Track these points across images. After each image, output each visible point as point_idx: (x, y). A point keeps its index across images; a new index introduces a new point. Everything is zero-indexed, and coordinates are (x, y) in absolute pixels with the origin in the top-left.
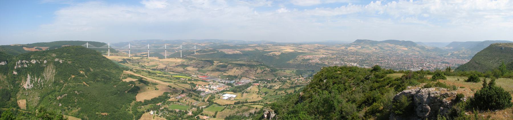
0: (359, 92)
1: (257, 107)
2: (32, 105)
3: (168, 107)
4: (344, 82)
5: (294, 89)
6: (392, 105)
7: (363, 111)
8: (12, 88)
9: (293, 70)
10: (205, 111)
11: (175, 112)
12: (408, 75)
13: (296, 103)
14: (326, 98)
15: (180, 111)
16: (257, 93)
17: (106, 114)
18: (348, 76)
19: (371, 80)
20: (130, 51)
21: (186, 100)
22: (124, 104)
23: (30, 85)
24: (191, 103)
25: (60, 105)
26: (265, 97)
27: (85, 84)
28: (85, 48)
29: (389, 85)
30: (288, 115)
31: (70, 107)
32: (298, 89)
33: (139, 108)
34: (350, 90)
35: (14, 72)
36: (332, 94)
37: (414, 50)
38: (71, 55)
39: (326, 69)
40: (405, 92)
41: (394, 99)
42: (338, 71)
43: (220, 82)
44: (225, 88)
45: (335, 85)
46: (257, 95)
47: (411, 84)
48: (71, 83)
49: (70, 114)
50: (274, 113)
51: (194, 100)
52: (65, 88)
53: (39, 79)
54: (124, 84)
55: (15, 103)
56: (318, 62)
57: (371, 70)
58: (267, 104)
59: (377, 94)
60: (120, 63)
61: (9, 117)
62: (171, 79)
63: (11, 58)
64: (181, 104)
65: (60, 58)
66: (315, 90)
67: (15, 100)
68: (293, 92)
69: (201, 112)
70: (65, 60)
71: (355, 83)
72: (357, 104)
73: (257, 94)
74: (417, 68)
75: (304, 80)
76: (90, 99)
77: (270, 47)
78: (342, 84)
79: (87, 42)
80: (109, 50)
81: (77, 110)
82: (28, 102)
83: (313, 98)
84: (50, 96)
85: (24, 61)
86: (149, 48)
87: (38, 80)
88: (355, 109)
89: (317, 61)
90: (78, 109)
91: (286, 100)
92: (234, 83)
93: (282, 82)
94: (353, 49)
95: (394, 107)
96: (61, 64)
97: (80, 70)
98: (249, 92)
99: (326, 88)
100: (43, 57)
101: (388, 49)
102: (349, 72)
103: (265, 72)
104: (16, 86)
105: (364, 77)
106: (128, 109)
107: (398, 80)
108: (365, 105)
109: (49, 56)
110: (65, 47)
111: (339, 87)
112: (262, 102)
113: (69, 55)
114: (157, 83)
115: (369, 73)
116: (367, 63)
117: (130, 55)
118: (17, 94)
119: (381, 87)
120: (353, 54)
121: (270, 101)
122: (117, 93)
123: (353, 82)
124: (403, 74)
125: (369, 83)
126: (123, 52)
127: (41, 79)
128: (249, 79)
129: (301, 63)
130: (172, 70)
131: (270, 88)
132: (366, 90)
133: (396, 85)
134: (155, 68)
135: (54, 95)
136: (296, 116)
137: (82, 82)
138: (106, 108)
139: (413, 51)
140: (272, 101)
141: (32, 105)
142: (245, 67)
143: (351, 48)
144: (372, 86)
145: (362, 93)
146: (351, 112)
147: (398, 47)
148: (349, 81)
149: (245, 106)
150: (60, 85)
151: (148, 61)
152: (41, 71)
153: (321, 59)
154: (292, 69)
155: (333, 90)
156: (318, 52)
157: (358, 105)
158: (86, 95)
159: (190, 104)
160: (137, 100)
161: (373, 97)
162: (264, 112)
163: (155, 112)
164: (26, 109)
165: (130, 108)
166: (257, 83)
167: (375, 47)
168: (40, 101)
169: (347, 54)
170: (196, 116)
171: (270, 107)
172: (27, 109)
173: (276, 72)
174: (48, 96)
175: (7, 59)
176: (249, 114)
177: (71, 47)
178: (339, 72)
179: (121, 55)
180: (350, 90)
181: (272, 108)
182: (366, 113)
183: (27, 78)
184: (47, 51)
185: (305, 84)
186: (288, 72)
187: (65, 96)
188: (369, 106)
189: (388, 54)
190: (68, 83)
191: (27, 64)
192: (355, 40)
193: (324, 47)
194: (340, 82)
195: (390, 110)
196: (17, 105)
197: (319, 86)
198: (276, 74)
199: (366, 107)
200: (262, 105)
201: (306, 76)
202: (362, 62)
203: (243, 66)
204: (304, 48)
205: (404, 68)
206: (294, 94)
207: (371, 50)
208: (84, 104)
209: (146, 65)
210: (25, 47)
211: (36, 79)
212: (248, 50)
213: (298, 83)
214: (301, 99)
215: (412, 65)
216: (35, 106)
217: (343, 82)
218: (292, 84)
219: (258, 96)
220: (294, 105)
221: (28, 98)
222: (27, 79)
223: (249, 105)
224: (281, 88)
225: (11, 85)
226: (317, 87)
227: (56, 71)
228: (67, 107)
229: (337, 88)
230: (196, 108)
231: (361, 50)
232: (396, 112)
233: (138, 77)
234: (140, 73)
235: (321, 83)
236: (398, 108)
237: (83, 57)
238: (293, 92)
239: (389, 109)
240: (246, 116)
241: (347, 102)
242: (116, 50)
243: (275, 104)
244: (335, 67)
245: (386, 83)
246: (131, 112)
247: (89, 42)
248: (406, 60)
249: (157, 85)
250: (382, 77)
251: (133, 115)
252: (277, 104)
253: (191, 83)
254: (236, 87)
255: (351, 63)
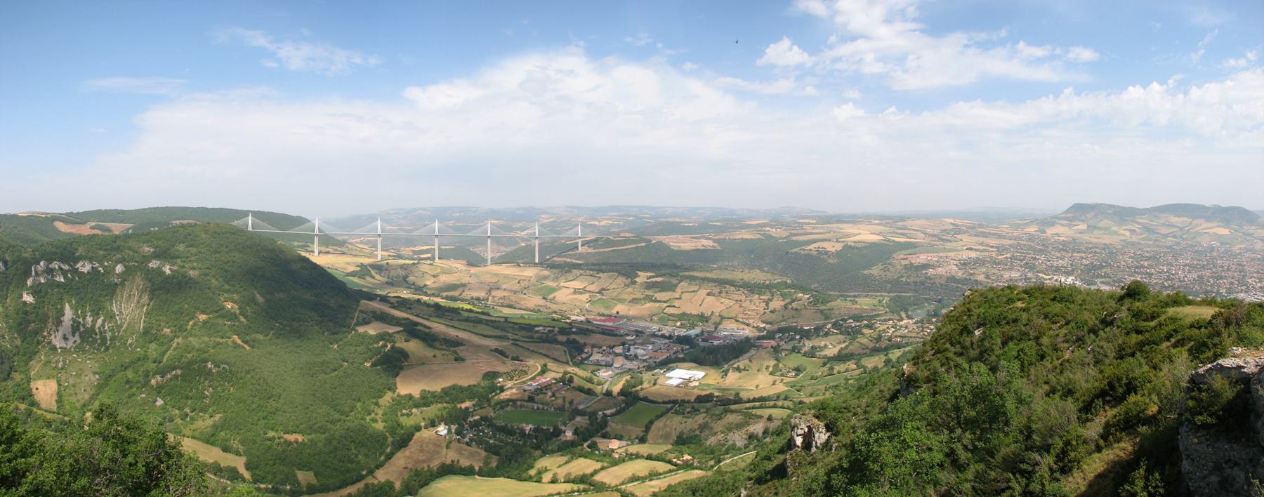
0: (1083, 365)
1: (770, 416)
2: (73, 399)
3: (492, 414)
4: (1036, 335)
5: (886, 355)
6: (1187, 399)
7: (1097, 421)
8: (18, 342)
9: (881, 296)
10: (613, 426)
11: (523, 433)
12: (1233, 312)
13: (893, 397)
14: (981, 385)
15: (537, 430)
16: (771, 369)
17: (300, 438)
18: (1050, 316)
19: (1118, 327)
20: (379, 240)
21: (554, 395)
22: (359, 401)
23: (70, 337)
24: (571, 402)
25: (160, 402)
26: (797, 382)
27: (239, 342)
28: (243, 231)
29: (1173, 340)
30: (870, 433)
31: (187, 410)
32: (895, 354)
33: (403, 415)
34: (1055, 359)
35: (25, 295)
36: (1002, 375)
37: (1251, 235)
38: (200, 252)
39: (982, 295)
40: (1223, 364)
41: (1192, 380)
42: (1019, 300)
43: (657, 336)
44: (672, 352)
45: (1011, 344)
46: (771, 377)
47: (1242, 340)
48: (195, 336)
49: (187, 431)
50: (824, 430)
51: (581, 391)
52: (175, 353)
53: (100, 321)
54: (361, 340)
55: (23, 389)
56: (953, 273)
57: (1118, 295)
58: (801, 403)
59: (1138, 367)
60: (351, 278)
61: (8, 427)
62: (503, 330)
63: (16, 254)
64: (541, 406)
65: (166, 258)
66: (947, 358)
67: (24, 381)
68: (880, 365)
69: (603, 429)
70: (180, 266)
71: (1069, 337)
72: (1078, 399)
73: (771, 373)
74: (1258, 293)
75: (915, 326)
76: (252, 390)
77: (808, 228)
78: (1030, 340)
79: (249, 211)
80: (316, 240)
81: (210, 422)
82: (62, 389)
83: (938, 384)
84: (130, 374)
85: (55, 265)
86: (437, 233)
87: (94, 322)
88: (1074, 417)
89: (951, 269)
90: (212, 419)
91: (860, 389)
92: (697, 335)
93: (849, 334)
94: (1062, 232)
95: (1191, 403)
96: (169, 277)
97: (225, 298)
98: (744, 370)
99: (981, 353)
100: (114, 253)
101: (1170, 231)
102: (1051, 303)
103: (793, 304)
104: (29, 339)
105: (1097, 318)
106: (373, 415)
107: (1200, 328)
108: (1103, 404)
109: (131, 253)
110: (183, 226)
111: (1022, 350)
112: (785, 399)
113: (193, 252)
114: (460, 341)
115: (1113, 304)
116: (1106, 276)
117: (379, 253)
118: (31, 363)
119: (1149, 345)
120: (1064, 247)
121: (811, 395)
122: (342, 366)
123: (1066, 335)
124: (1217, 310)
125: (1115, 335)
126: (361, 242)
127: (104, 321)
128: (746, 327)
129: (902, 277)
130: (507, 302)
131: (811, 354)
132: (1106, 356)
133: (1193, 343)
134: (457, 295)
135: (140, 373)
136: (895, 436)
137: (228, 335)
138: (308, 408)
139: (1246, 237)
140: (818, 395)
141: (73, 399)
142: (732, 288)
143: (1057, 229)
144: (1124, 343)
145: (1092, 366)
146: (1061, 426)
147: (1201, 225)
148: (1051, 332)
149: (732, 412)
150: (161, 340)
151: (435, 273)
152: (106, 296)
153: (964, 264)
154: (879, 294)
155: (1003, 362)
156: (955, 244)
157: (1081, 405)
158: (239, 375)
159: (567, 405)
160: (397, 391)
161: (1127, 378)
162: (793, 428)
163: (454, 428)
164: (55, 410)
165: (376, 414)
166: (769, 339)
167: (1130, 227)
168: (100, 387)
169: (1044, 247)
170: (586, 441)
171: (813, 411)
172: (58, 407)
173: (828, 305)
174: (122, 373)
175: (6, 255)
176: (745, 436)
177: (199, 225)
178: (1019, 304)
179: (354, 253)
180: (1055, 359)
181: (817, 417)
182: (1107, 426)
183: (63, 315)
184: (126, 237)
185: (918, 339)
186: (866, 305)
187: (176, 377)
188: (1114, 406)
189: (1170, 247)
190: (185, 338)
191: (64, 273)
192: (1069, 206)
193: (972, 228)
194: (1024, 336)
195: (1180, 415)
196: (31, 396)
197: (958, 346)
198: (829, 310)
199: (1107, 408)
200: (788, 408)
201: (920, 314)
202: (1089, 271)
203: (728, 286)
204: (914, 230)
205: (1218, 292)
206: (884, 369)
207: (1118, 235)
208: (233, 403)
209: (428, 283)
210: (61, 221)
211: (89, 319)
212: (740, 237)
213: (896, 337)
214: (907, 386)
215: (1242, 282)
216: (82, 402)
217: (1032, 334)
218: (879, 338)
219: (775, 381)
220: (885, 403)
221: (63, 376)
222: (62, 319)
223: (746, 409)
224: (844, 352)
225: (16, 335)
226: (952, 349)
227: (151, 300)
228: (179, 409)
229: (1015, 353)
230: (586, 417)
231: (1086, 237)
232: (1199, 419)
233: (403, 322)
234: (410, 308)
235: (967, 340)
236: (1204, 407)
237: (235, 259)
238: (880, 365)
239: (1178, 410)
240: (737, 443)
241: (1047, 395)
242: (340, 238)
243: (828, 402)
244: (1009, 287)
245: (1163, 333)
246: (380, 426)
247: (257, 214)
248: (1223, 267)
249: (461, 348)
250: (1153, 318)
251: (387, 434)
252: (833, 404)
253: (568, 341)
254: (704, 349)
255: (1056, 277)
